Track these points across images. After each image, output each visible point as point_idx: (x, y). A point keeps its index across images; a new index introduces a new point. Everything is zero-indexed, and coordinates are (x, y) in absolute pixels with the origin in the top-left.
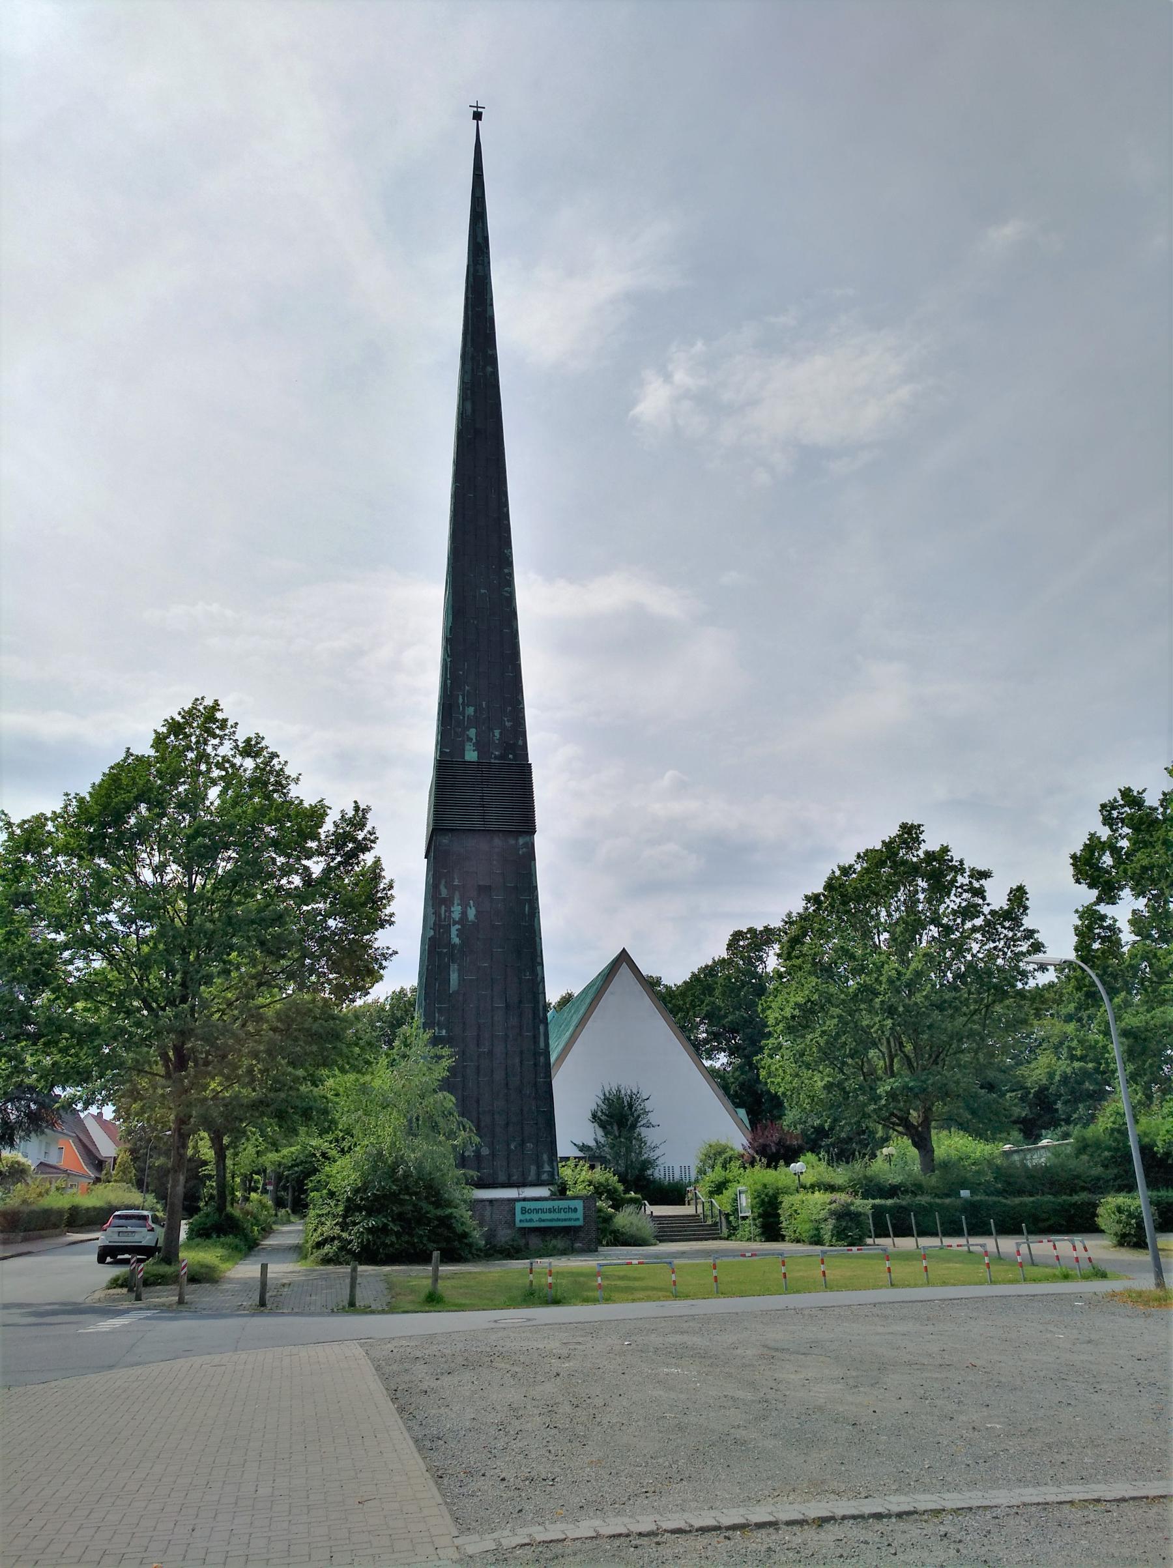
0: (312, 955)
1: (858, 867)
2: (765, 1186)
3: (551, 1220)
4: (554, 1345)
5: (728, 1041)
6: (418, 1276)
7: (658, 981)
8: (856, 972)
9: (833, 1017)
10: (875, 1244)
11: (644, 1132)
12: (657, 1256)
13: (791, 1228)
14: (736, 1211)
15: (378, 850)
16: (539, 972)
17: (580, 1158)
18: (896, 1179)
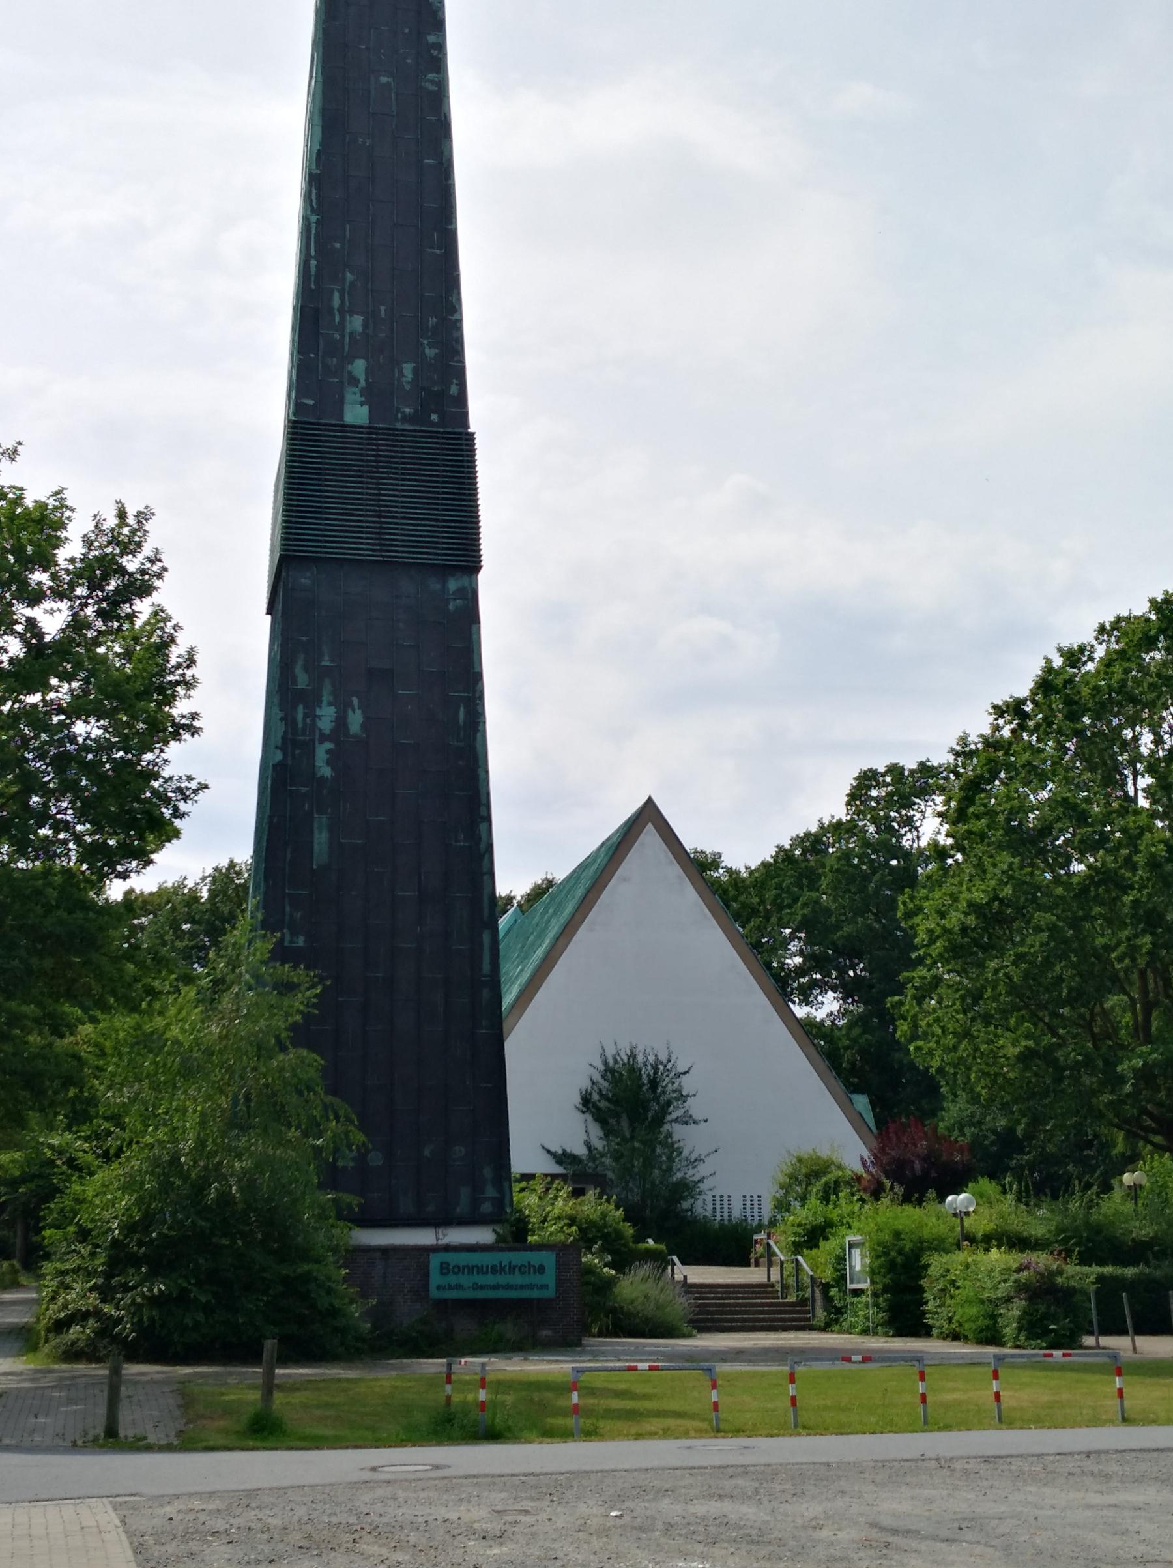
0: (46, 792)
1: (1100, 652)
2: (897, 1234)
3: (496, 1287)
4: (477, 1514)
5: (842, 972)
6: (238, 1385)
7: (714, 862)
8: (1085, 847)
9: (1038, 929)
10: (1098, 1346)
11: (679, 1132)
12: (691, 1359)
13: (944, 1313)
14: (841, 1280)
15: (165, 595)
16: (484, 836)
17: (554, 1177)
18: (1143, 1230)
